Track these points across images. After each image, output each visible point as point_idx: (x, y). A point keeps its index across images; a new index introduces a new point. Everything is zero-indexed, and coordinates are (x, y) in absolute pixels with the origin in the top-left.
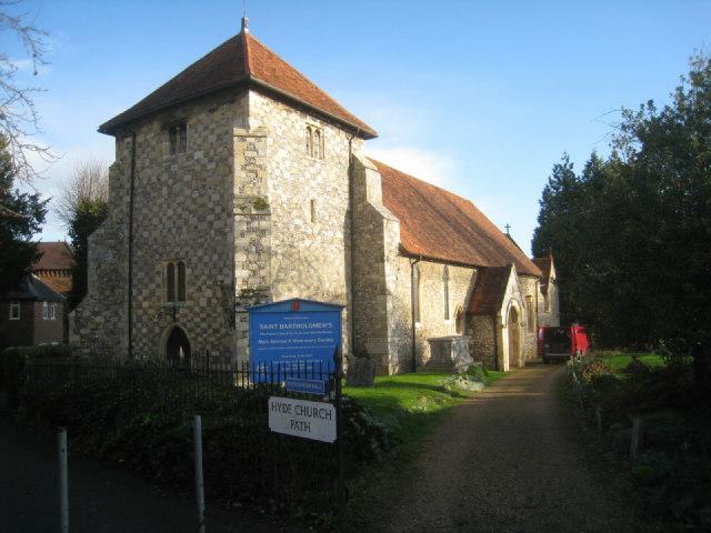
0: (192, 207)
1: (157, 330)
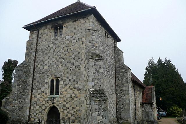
0: (64, 57)
1: (44, 107)
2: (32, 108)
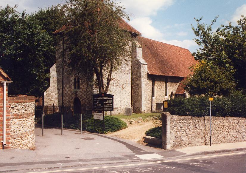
1: (71, 98)
2: (64, 98)
